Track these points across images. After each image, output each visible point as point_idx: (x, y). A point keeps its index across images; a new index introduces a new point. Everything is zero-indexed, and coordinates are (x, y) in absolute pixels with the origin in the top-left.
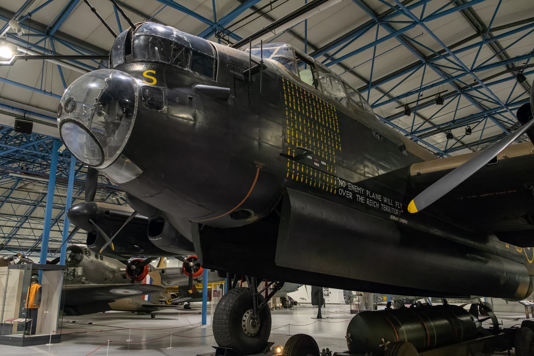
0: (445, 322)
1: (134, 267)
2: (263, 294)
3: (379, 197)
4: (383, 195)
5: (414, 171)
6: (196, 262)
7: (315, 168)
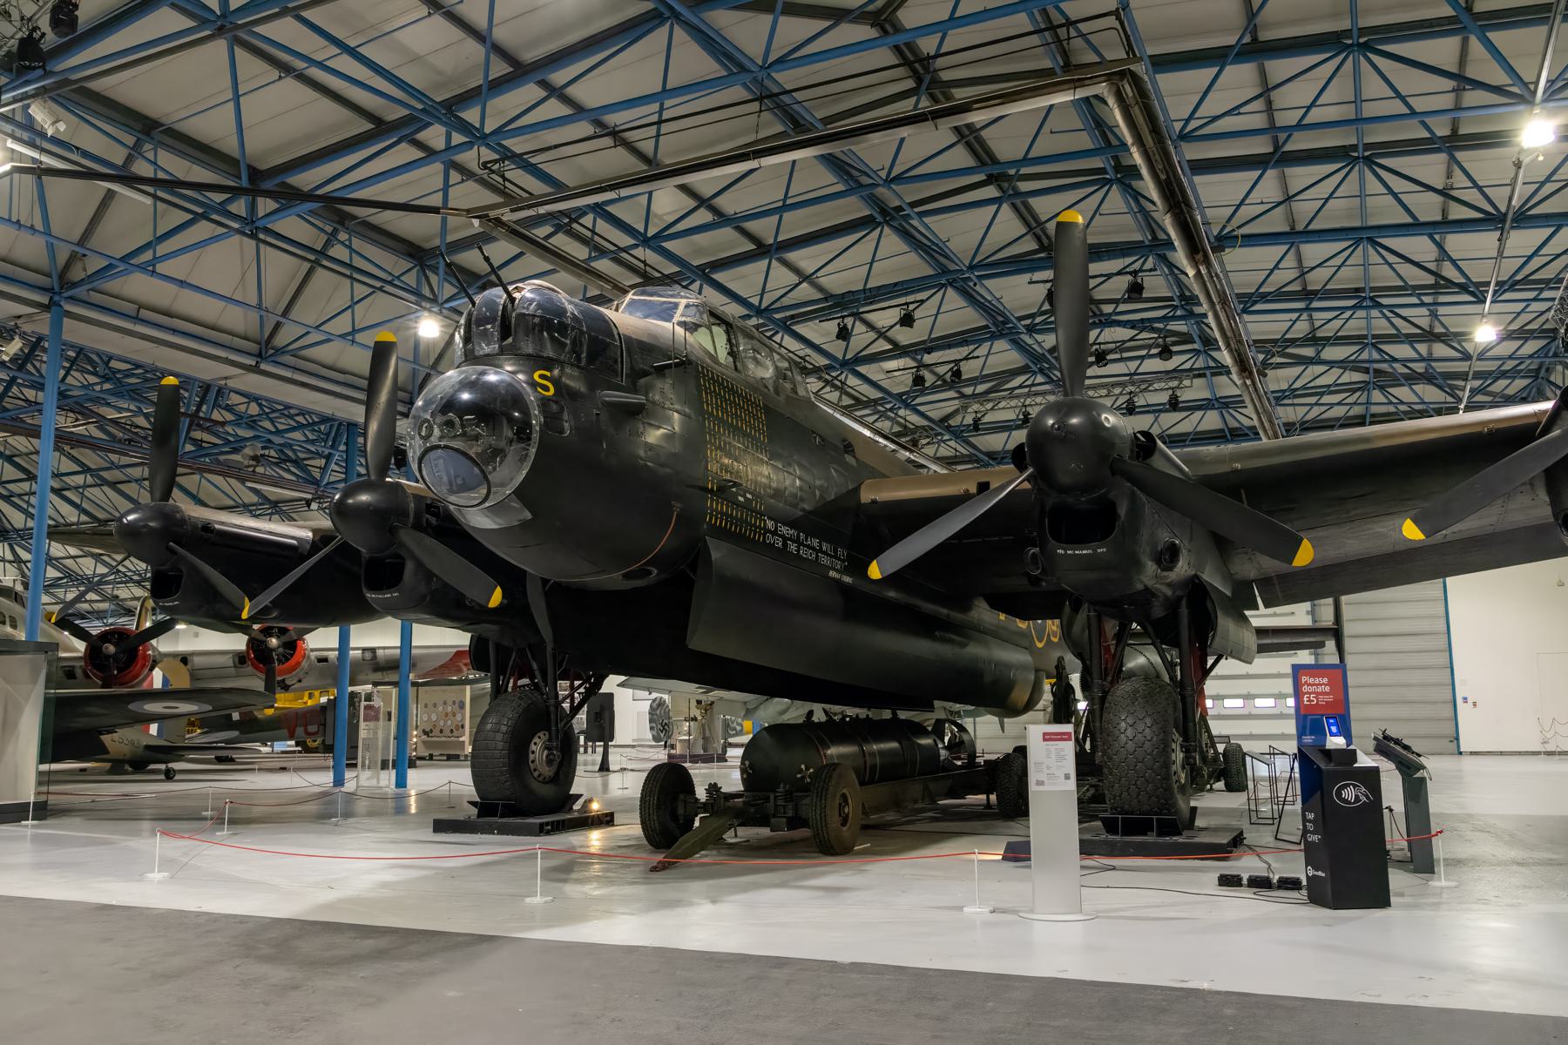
0: (894, 745)
1: (111, 649)
2: (566, 705)
3: (815, 542)
4: (822, 539)
5: (866, 496)
6: (285, 638)
7: (738, 505)
